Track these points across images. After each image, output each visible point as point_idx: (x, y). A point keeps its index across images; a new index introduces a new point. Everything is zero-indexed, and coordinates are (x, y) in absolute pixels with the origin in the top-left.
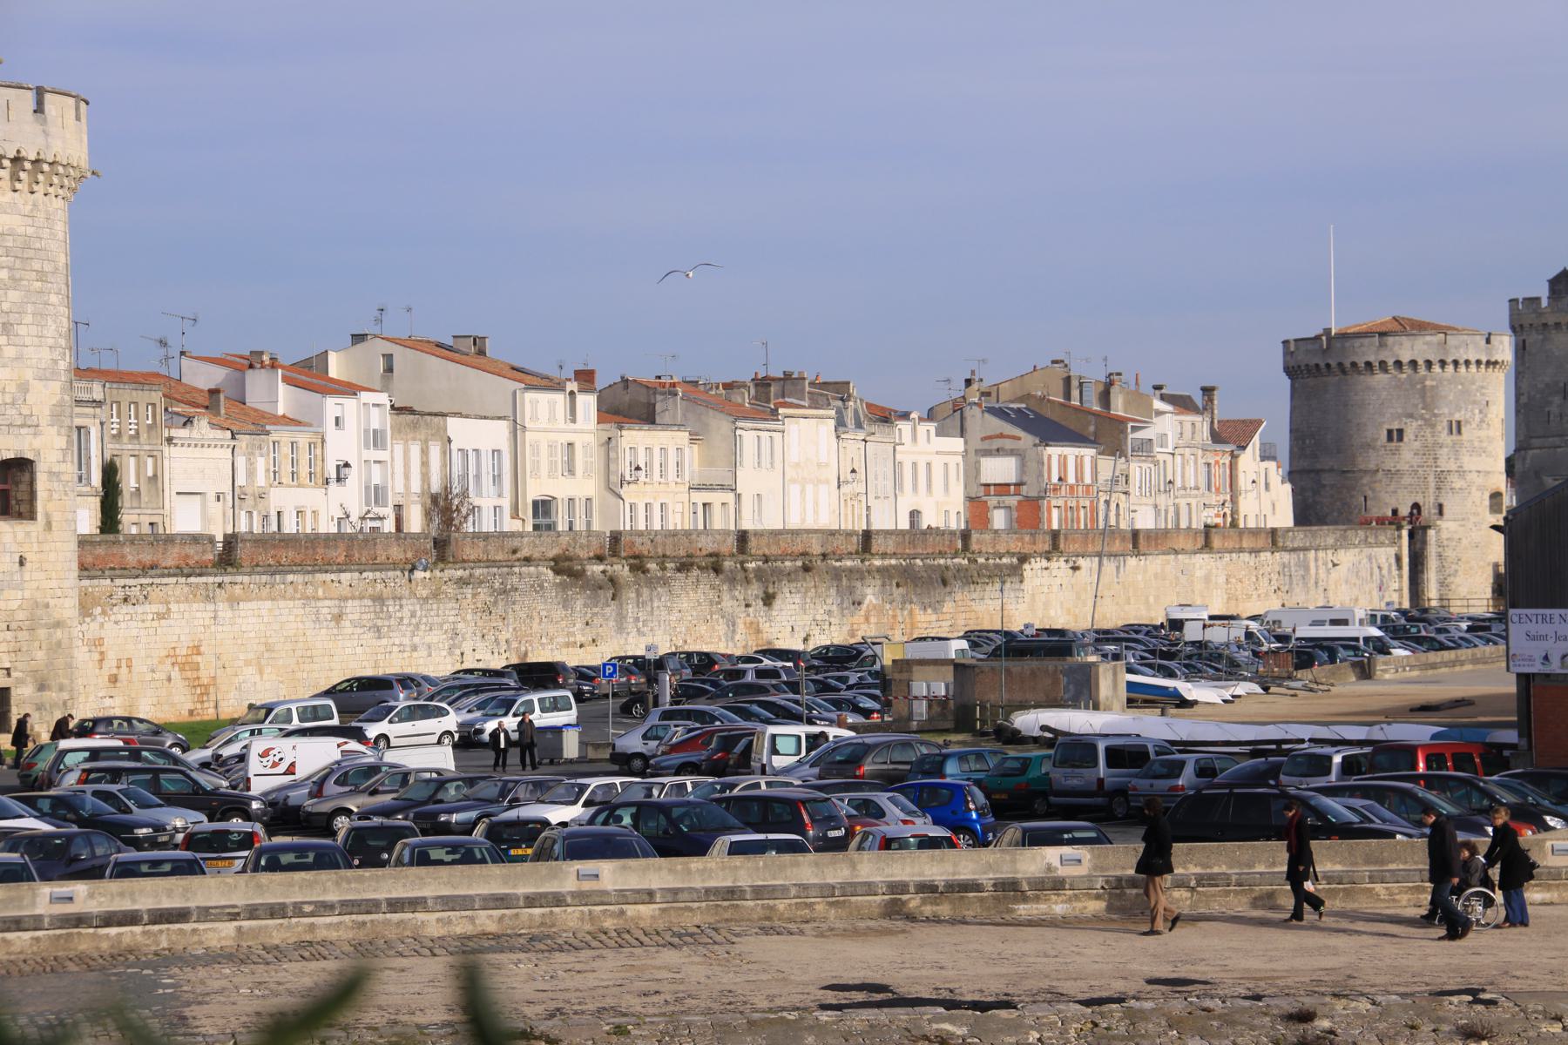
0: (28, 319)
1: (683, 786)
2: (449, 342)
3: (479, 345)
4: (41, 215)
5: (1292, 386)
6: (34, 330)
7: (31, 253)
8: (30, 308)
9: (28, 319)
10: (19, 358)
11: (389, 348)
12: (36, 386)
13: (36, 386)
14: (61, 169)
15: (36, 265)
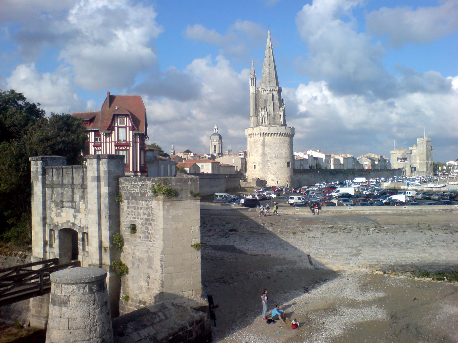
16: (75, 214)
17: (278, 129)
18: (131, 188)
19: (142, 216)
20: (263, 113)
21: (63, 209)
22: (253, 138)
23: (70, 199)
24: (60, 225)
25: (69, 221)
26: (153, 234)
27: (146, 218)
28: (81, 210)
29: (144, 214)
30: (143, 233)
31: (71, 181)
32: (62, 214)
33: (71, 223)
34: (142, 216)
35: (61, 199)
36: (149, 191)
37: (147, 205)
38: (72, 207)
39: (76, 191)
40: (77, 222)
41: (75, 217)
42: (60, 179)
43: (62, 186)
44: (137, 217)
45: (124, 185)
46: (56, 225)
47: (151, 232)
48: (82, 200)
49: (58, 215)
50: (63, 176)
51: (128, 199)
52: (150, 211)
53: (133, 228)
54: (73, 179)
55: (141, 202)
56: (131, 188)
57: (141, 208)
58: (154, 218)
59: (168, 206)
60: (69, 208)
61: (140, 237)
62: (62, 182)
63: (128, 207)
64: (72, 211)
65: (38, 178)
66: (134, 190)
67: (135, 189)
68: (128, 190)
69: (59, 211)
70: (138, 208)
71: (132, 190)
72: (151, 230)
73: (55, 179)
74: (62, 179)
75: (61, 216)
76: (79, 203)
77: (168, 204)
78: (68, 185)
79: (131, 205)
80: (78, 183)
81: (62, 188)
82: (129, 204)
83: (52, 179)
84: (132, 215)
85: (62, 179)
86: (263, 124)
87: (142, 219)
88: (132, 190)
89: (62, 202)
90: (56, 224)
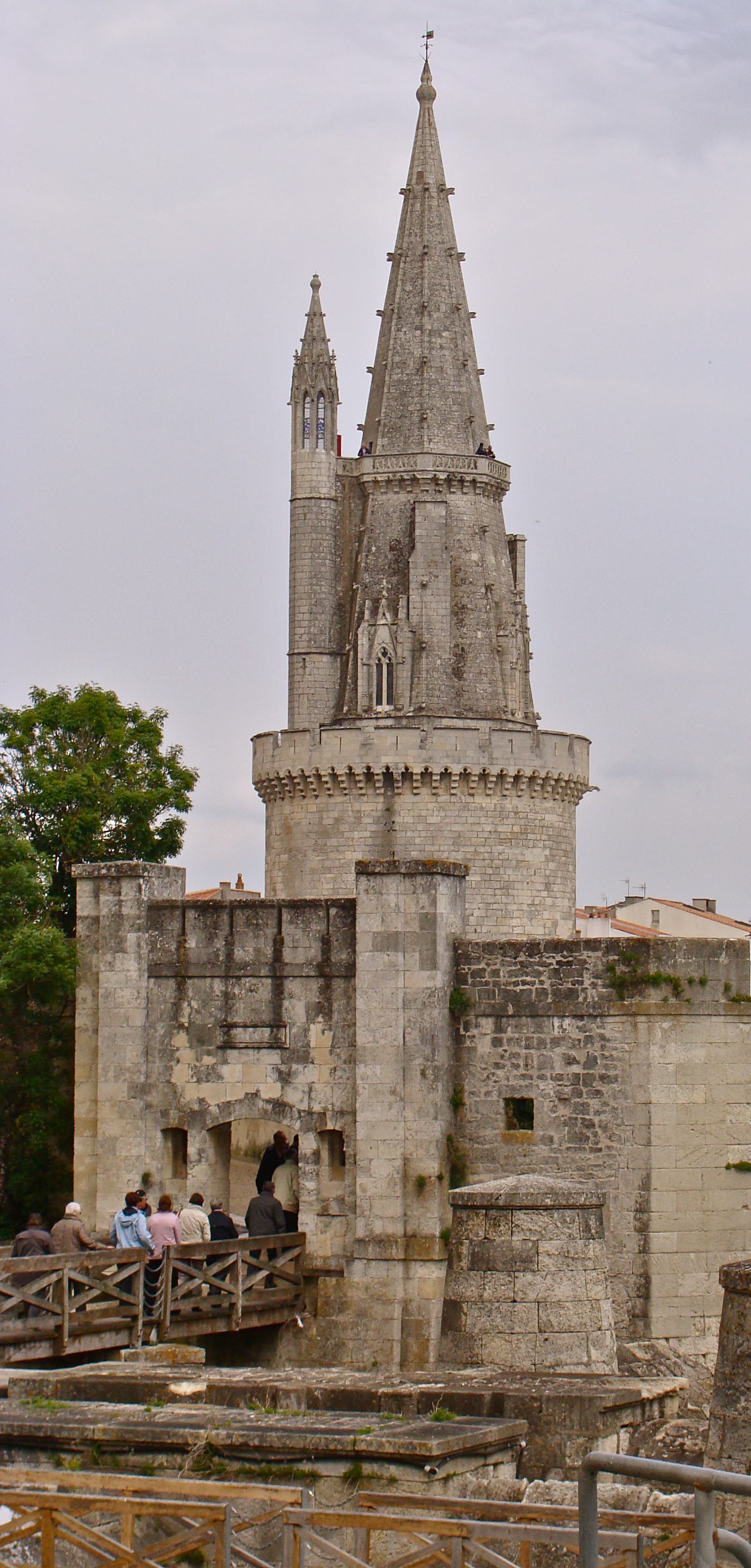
0: (559, 881)
1: (320, 1439)
2: (691, 903)
3: (710, 905)
4: (567, 815)
5: (404, 211)
6: (561, 888)
7: (560, 839)
8: (560, 874)
9: (559, 881)
10: (553, 905)
11: (656, 906)
12: (561, 922)
13: (561, 922)
14: (572, 785)
15: (563, 847)
16: (283, 1068)
17: (484, 747)
18: (511, 974)
19: (559, 1068)
20: (383, 634)
21: (232, 1054)
22: (312, 805)
23: (266, 1017)
24: (214, 1109)
25: (256, 1094)
26: (605, 1128)
27: (577, 1076)
28: (313, 1054)
29: (570, 1061)
30: (565, 1124)
31: (269, 951)
32: (225, 1070)
33: (268, 1101)
34: (559, 1068)
35: (221, 1016)
36: (594, 985)
37: (581, 1029)
38: (275, 1045)
39: (292, 986)
40: (294, 1097)
41: (285, 1078)
42: (219, 943)
43: (231, 971)
44: (534, 1073)
45: (482, 965)
46: (193, 1112)
47: (596, 1120)
48: (320, 1019)
49: (209, 1075)
50: (231, 933)
51: (498, 1015)
52: (595, 1049)
53: (521, 1112)
54: (278, 943)
55: (556, 1022)
56: (511, 974)
57: (556, 1042)
58: (612, 1073)
59: (664, 1031)
60: (258, 1047)
61: (551, 1139)
62: (230, 955)
63: (497, 1042)
64: (273, 1057)
65: (121, 941)
66: (524, 983)
67: (528, 979)
68: (496, 984)
69: (208, 1060)
70: (542, 1043)
71: (516, 984)
72: (597, 1113)
73: (192, 943)
74: (230, 944)
75: (220, 1077)
76: (306, 1030)
77: (665, 1025)
78: (256, 963)
79: (510, 1033)
80: (301, 959)
81: (226, 977)
82: (499, 1029)
83: (181, 944)
84: (517, 1066)
85: (230, 944)
86: (384, 708)
87: (559, 1078)
88: (516, 984)
89: (228, 1027)
90: (196, 1107)
